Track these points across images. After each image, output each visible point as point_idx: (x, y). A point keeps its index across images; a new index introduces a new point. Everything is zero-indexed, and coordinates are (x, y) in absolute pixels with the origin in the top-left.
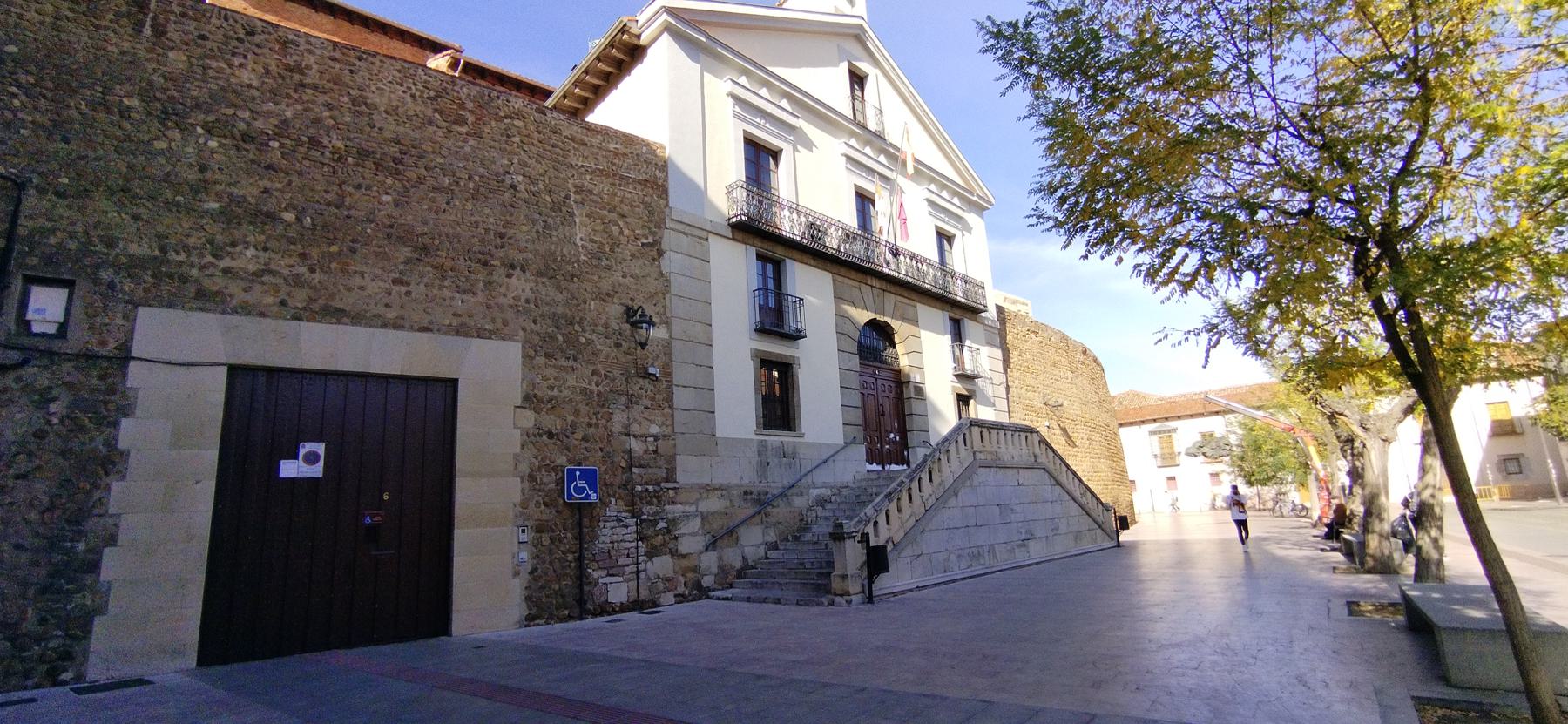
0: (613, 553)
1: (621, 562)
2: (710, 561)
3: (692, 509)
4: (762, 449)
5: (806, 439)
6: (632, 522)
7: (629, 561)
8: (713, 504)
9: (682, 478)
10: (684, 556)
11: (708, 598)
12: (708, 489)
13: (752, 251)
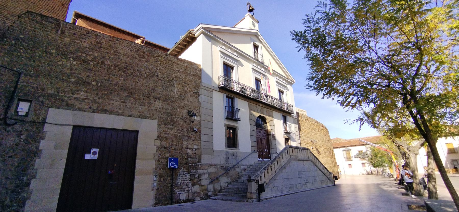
0: (182, 184)
1: (184, 187)
2: (211, 187)
3: (206, 171)
4: (227, 153)
5: (240, 151)
6: (188, 175)
7: (187, 187)
8: (212, 170)
9: (203, 162)
10: (203, 186)
11: (210, 199)
12: (211, 165)
13: (225, 95)
